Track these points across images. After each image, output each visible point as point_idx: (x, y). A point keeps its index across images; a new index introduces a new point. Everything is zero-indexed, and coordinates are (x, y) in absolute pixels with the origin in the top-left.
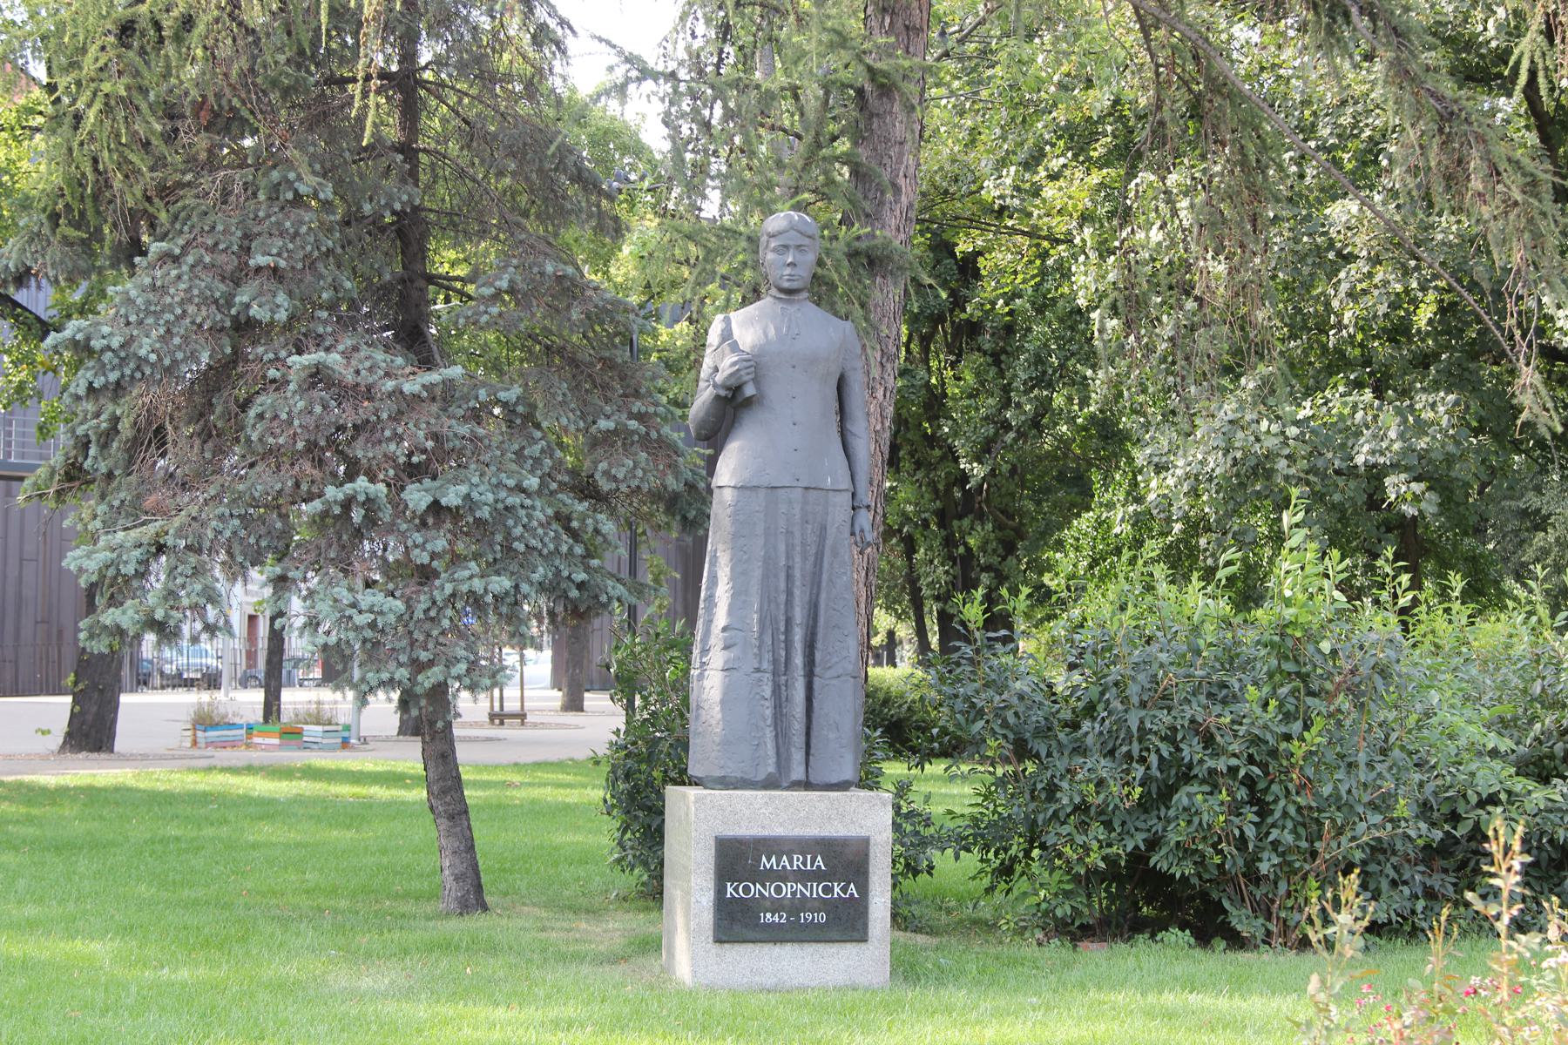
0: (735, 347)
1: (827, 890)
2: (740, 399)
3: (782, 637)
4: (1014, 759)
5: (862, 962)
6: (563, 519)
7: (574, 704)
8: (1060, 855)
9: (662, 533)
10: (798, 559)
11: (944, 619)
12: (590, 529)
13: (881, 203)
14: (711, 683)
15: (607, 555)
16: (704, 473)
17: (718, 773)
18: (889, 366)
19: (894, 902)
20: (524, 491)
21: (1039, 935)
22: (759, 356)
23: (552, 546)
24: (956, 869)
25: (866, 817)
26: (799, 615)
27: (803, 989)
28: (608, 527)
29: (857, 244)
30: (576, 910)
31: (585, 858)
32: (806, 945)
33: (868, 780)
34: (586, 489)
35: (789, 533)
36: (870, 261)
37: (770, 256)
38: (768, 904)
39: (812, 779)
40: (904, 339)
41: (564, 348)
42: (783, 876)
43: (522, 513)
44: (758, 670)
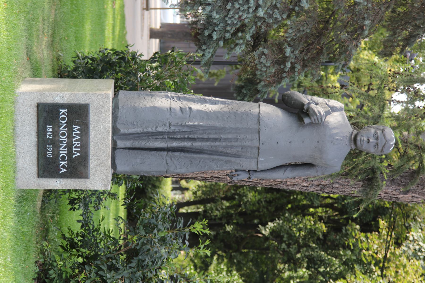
0: (328, 113)
1: (63, 158)
2: (302, 116)
3: (186, 136)
4: (126, 249)
5: (27, 174)
6: (242, 28)
7: (153, 34)
8: (80, 272)
9: (237, 77)
10: (224, 144)
11: (195, 216)
12: (237, 42)
13: (399, 185)
14: (163, 101)
15: (226, 50)
16: (265, 97)
17: (120, 105)
18: (318, 188)
19: (56, 191)
20: (257, 8)
21: (42, 261)
22: (324, 124)
23: (229, 22)
24: (73, 220)
25: (99, 177)
26: (197, 144)
27: (15, 147)
28: (238, 51)
29: (379, 172)
30: (53, 35)
31: (79, 39)
32: (36, 148)
33: (117, 179)
34: (259, 39)
35: (237, 140)
36: (370, 179)
37: (373, 131)
38: (56, 129)
39: (117, 151)
40: (332, 195)
41: (327, 30)
42: (70, 136)
43: (246, 7)
44: (170, 124)
